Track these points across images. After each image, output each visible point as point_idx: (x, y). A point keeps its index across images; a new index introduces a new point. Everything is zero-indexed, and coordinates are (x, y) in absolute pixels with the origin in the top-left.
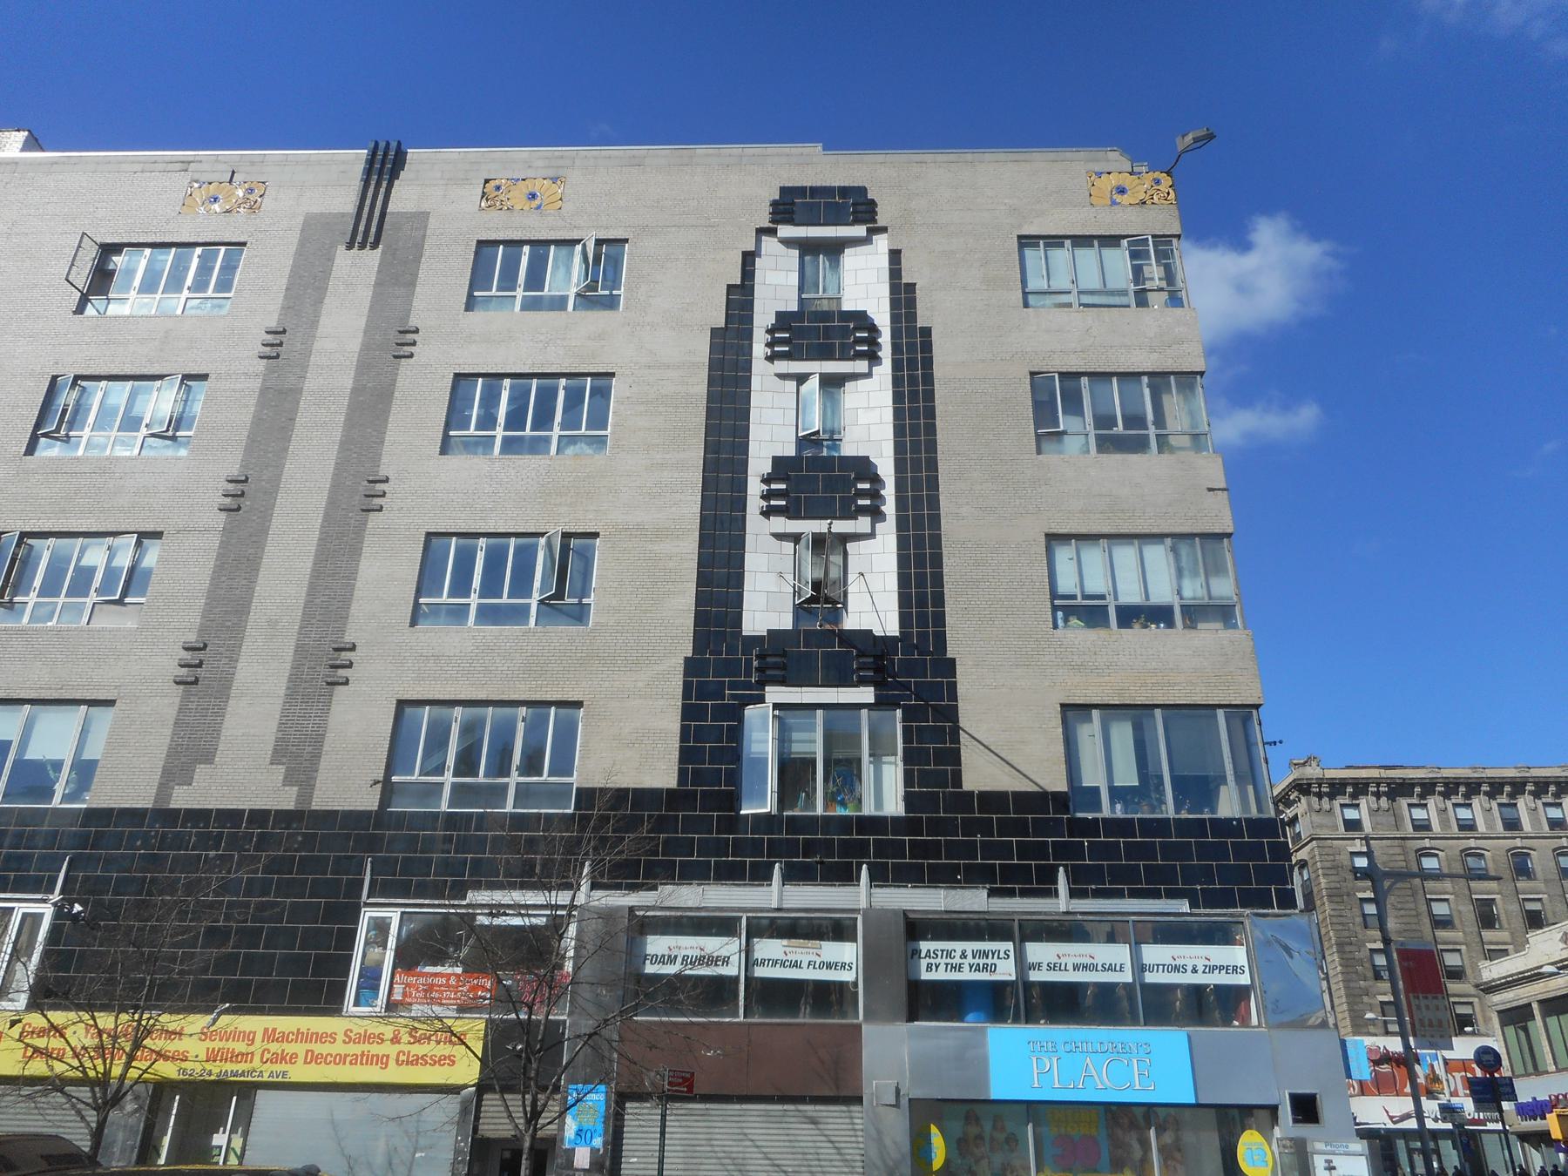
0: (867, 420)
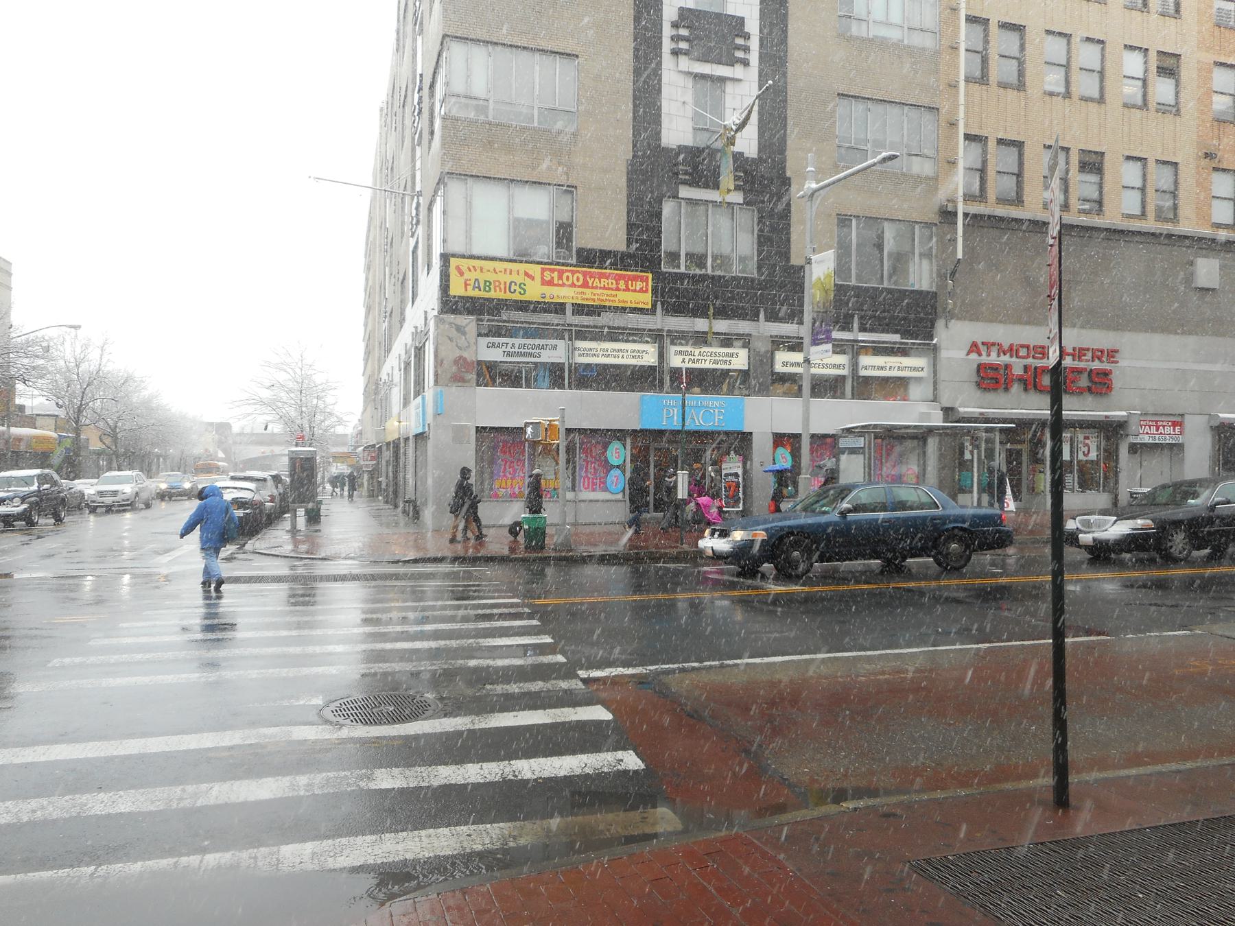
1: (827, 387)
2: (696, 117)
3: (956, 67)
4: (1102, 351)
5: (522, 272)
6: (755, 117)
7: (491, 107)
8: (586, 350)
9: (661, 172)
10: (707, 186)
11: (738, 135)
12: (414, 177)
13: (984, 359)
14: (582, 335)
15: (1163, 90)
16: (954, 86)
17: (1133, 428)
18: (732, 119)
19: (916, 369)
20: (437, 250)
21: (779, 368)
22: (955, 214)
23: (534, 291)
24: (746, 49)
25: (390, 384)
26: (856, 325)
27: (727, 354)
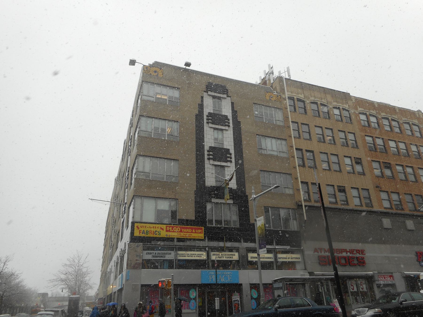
0: (228, 141)
1: (267, 266)
2: (216, 177)
3: (295, 162)
4: (359, 250)
5: (159, 228)
6: (234, 177)
7: (151, 175)
8: (181, 254)
9: (205, 193)
10: (221, 198)
11: (230, 182)
12: (124, 198)
13: (320, 254)
14: (181, 249)
15: (358, 168)
16: (295, 168)
17: (376, 278)
18: (228, 178)
19: (297, 258)
20: (131, 220)
21: (250, 259)
22: (302, 205)
23: (164, 234)
24: (231, 158)
25: (111, 272)
26: (274, 244)
27: (231, 255)
